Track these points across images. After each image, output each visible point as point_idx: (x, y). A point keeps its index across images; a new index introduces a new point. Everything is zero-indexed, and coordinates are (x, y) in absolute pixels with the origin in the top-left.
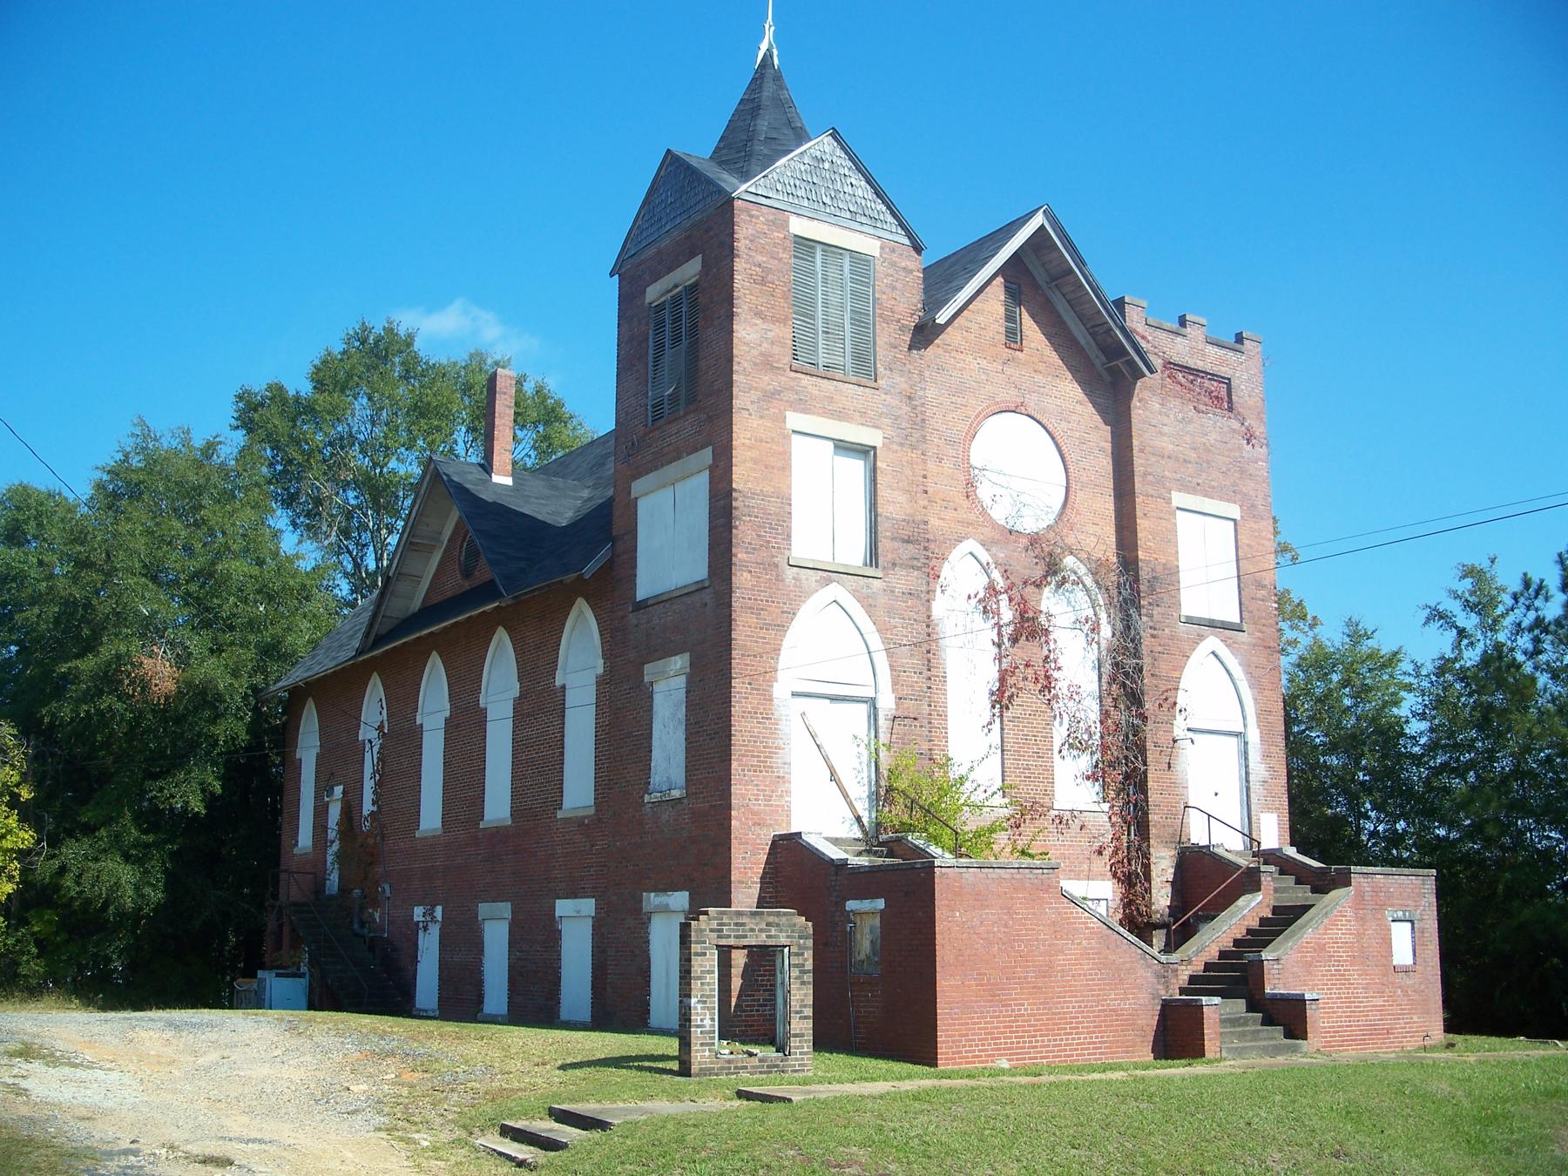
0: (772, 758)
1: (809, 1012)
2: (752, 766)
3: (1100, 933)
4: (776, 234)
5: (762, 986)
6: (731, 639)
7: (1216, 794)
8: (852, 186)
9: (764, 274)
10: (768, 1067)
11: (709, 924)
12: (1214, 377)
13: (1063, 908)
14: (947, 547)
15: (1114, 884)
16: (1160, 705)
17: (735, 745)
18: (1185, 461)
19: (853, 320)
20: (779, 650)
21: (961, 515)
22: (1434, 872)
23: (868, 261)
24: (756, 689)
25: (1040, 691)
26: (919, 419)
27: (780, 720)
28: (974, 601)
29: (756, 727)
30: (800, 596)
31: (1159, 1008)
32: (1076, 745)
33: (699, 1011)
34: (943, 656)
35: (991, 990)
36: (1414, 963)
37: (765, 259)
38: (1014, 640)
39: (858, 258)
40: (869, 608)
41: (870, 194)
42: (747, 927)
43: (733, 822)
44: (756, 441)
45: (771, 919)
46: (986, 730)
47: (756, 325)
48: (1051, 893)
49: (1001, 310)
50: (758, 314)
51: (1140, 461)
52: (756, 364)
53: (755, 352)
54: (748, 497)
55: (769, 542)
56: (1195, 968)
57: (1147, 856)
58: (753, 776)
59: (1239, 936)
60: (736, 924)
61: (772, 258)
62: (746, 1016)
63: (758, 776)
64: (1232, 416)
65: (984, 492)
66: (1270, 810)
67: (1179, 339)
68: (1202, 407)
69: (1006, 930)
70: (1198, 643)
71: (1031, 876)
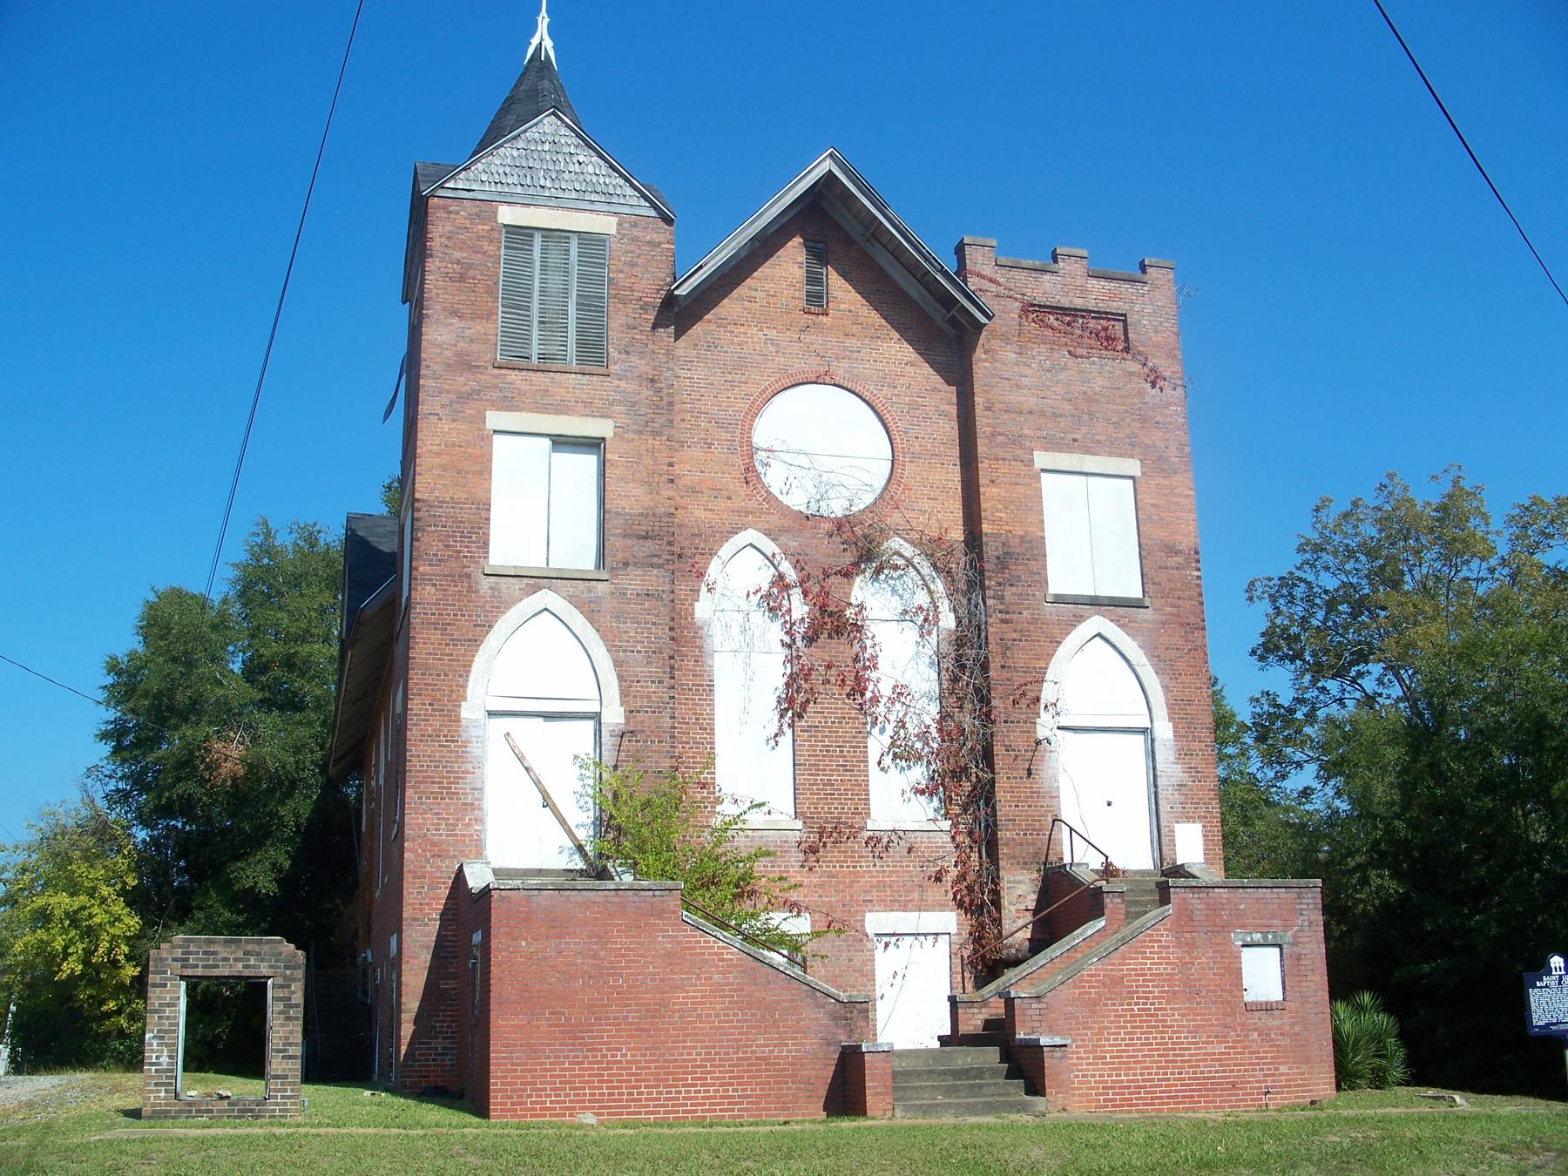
0: (458, 783)
1: (297, 1051)
2: (432, 793)
3: (742, 965)
4: (480, 227)
5: (441, 1033)
6: (408, 658)
7: (1109, 804)
8: (580, 164)
9: (463, 271)
10: (239, 1111)
11: (171, 953)
12: (1101, 315)
13: (685, 936)
15: (958, 915)
17: (410, 771)
19: (580, 306)
20: (470, 666)
21: (737, 503)
22: (1319, 882)
23: (605, 241)
24: (438, 710)
25: (848, 695)
26: (664, 403)
27: (470, 742)
28: (755, 599)
29: (438, 751)
31: (837, 1056)
32: (902, 754)
33: (155, 1047)
34: (710, 662)
35: (572, 1031)
36: (1284, 999)
37: (465, 255)
38: (810, 639)
40: (591, 615)
41: (605, 170)
42: (219, 957)
43: (406, 855)
44: (446, 446)
45: (250, 947)
46: (772, 743)
47: (451, 324)
48: (667, 918)
49: (800, 273)
50: (455, 313)
51: (985, 421)
52: (448, 365)
53: (448, 354)
54: (434, 506)
55: (459, 552)
56: (994, 1011)
57: (996, 880)
58: (433, 804)
61: (475, 252)
62: (418, 1066)
63: (439, 804)
64: (1129, 357)
65: (774, 478)
66: (1190, 819)
67: (1047, 277)
68: (1080, 351)
69: (594, 962)
70: (1075, 626)
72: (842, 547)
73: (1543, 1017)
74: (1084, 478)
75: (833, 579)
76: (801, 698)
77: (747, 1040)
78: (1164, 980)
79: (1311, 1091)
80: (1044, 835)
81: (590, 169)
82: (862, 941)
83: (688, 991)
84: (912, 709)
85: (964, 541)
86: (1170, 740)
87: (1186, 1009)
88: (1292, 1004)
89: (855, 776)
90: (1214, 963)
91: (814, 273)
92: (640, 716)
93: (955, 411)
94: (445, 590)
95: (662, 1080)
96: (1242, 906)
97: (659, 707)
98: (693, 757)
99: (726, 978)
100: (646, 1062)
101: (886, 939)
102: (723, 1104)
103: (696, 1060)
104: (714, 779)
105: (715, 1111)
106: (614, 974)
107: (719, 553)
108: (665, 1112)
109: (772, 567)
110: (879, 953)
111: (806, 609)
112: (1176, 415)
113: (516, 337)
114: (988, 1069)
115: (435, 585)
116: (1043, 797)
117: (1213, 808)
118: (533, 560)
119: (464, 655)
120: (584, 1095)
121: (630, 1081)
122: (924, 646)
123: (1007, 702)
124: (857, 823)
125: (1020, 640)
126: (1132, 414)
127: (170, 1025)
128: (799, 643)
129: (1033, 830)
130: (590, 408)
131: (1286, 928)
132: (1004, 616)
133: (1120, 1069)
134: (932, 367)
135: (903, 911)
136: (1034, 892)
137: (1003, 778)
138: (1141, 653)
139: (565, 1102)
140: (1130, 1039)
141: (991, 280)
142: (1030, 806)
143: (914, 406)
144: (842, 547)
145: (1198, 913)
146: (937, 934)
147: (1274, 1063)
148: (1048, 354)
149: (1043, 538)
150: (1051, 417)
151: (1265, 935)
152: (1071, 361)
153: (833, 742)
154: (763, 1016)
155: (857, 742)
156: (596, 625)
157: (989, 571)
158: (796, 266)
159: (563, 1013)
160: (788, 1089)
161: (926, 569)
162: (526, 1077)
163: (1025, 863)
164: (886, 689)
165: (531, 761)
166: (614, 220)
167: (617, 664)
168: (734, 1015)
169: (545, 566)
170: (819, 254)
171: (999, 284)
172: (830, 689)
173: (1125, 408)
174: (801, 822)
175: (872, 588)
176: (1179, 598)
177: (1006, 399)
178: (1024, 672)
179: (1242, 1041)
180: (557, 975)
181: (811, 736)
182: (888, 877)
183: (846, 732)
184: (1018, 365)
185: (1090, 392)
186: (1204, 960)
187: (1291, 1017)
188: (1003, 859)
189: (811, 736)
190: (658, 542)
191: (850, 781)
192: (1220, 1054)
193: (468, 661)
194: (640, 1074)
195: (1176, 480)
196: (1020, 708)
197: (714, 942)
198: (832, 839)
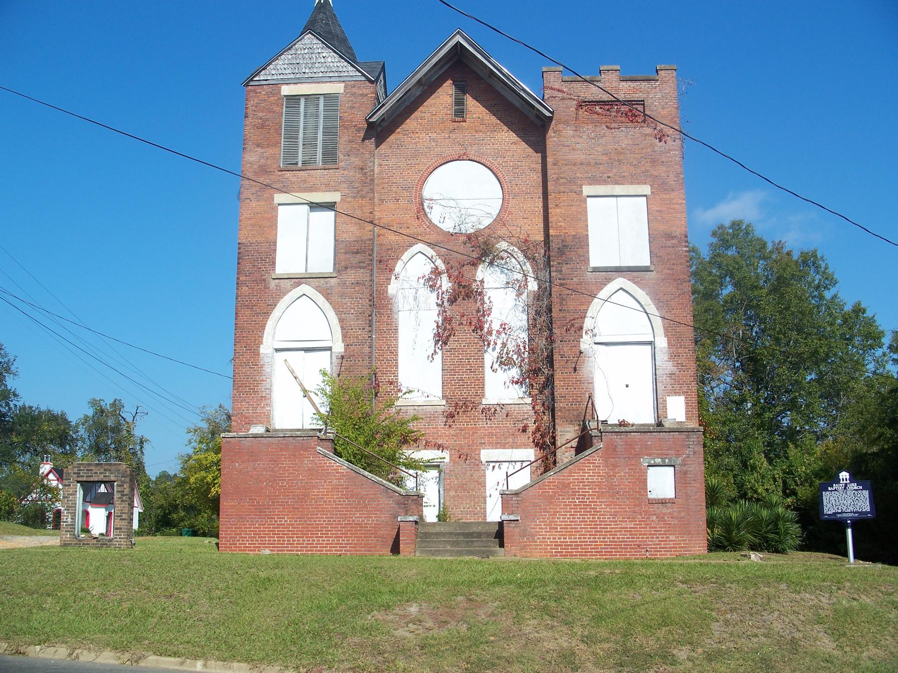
2: (245, 392)
3: (348, 475)
4: (272, 98)
7: (627, 386)
10: (101, 544)
13: (318, 460)
14: (400, 252)
15: (535, 450)
18: (596, 164)
20: (265, 326)
23: (338, 97)
24: (249, 350)
25: (473, 331)
28: (422, 281)
30: (279, 295)
32: (505, 362)
34: (396, 317)
37: (264, 114)
38: (453, 300)
39: (330, 98)
42: (93, 472)
46: (430, 359)
47: (257, 151)
51: (552, 171)
52: (256, 173)
53: (255, 167)
55: (260, 268)
60: (87, 470)
63: (249, 397)
65: (435, 215)
66: (677, 393)
68: (613, 125)
70: (605, 285)
71: (294, 441)
72: (471, 249)
73: (831, 509)
74: (615, 199)
75: (465, 267)
76: (447, 333)
77: (350, 514)
78: (596, 485)
79: (691, 551)
80: (583, 404)
81: (329, 60)
82: (478, 465)
83: (319, 489)
84: (511, 337)
85: (544, 241)
86: (665, 348)
87: (610, 502)
88: (680, 500)
89: (476, 375)
90: (629, 476)
91: (459, 99)
92: (352, 348)
93: (540, 167)
94: (253, 288)
95: (305, 534)
96: (649, 443)
97: (363, 342)
98: (386, 368)
99: (339, 482)
100: (297, 524)
101: (492, 464)
102: (337, 547)
103: (323, 524)
104: (398, 379)
105: (332, 551)
106: (281, 480)
107: (402, 258)
108: (306, 551)
109: (432, 263)
110: (489, 473)
111: (450, 284)
112: (675, 156)
113: (291, 153)
114: (484, 533)
115: (247, 286)
117: (692, 387)
118: (298, 269)
119: (262, 321)
120: (266, 541)
121: (289, 534)
122: (519, 301)
123: (562, 330)
124: (477, 400)
125: (572, 295)
126: (646, 158)
127: (72, 504)
128: (446, 304)
130: (328, 188)
131: (678, 456)
132: (562, 281)
133: (566, 535)
134: (526, 144)
135: (503, 448)
137: (559, 373)
138: (648, 298)
139: (256, 544)
140: (573, 518)
141: (558, 90)
142: (575, 389)
143: (515, 167)
144: (471, 249)
145: (619, 447)
146: (523, 461)
147: (666, 534)
148: (592, 129)
149: (587, 235)
150: (594, 166)
151: (663, 460)
152: (608, 132)
153: (464, 356)
154: (359, 501)
155: (478, 356)
156: (330, 301)
157: (553, 256)
158: (448, 96)
159: (256, 499)
160: (372, 540)
161: (521, 257)
162: (237, 531)
163: (571, 421)
164: (496, 326)
165: (297, 374)
166: (342, 85)
167: (341, 321)
168: (344, 501)
169: (304, 272)
170: (462, 88)
171: (563, 92)
172: (463, 328)
173: (641, 155)
174: (445, 401)
175: (490, 270)
176: (674, 264)
177: (567, 157)
178: (573, 313)
179: (645, 521)
180: (253, 480)
181: (451, 354)
182: (495, 430)
183: (472, 351)
184: (574, 137)
185: (619, 148)
186: (622, 474)
187: (679, 508)
188: (558, 419)
189: (451, 354)
190: (364, 255)
191: (474, 377)
192: (630, 528)
193: (264, 324)
194: (294, 531)
195: (674, 195)
196: (570, 333)
197: (334, 463)
198: (462, 410)
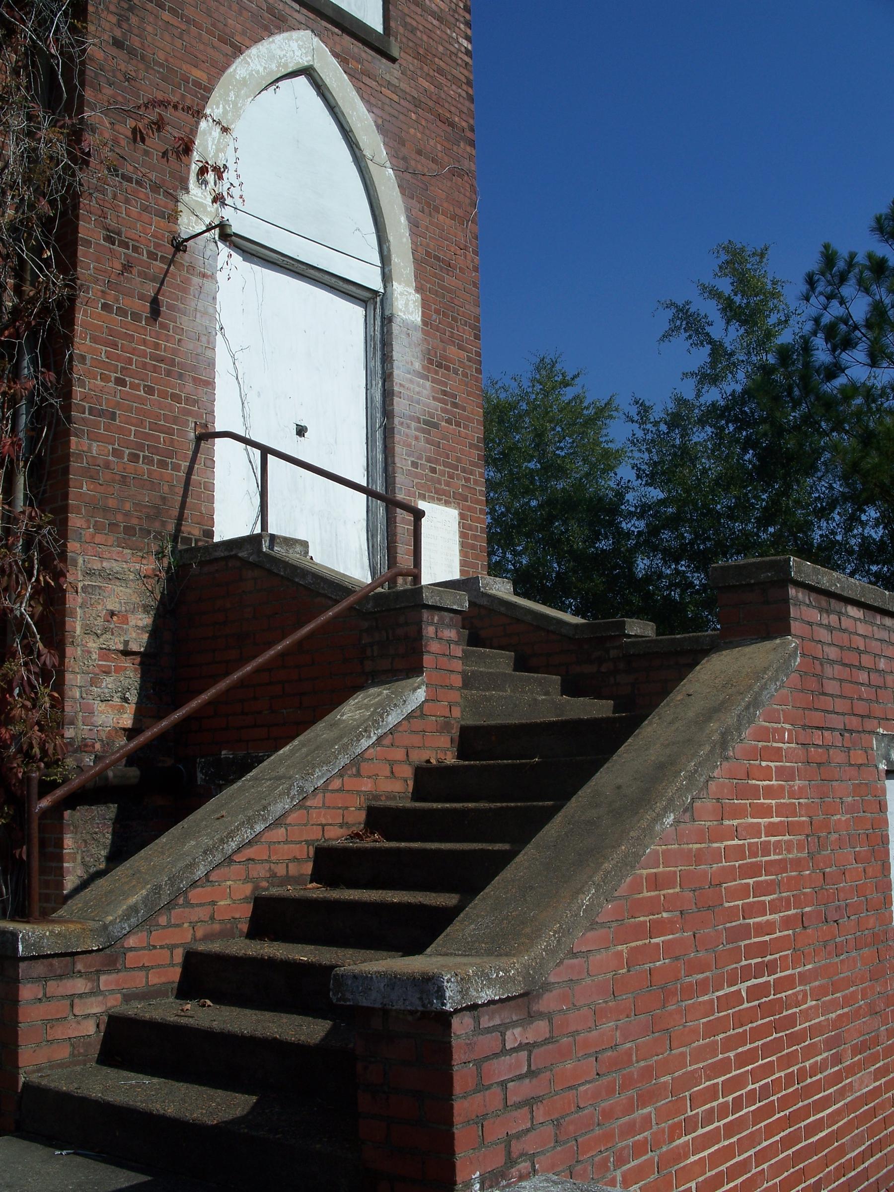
16: (137, 136)
56: (138, 981)
59: (336, 836)
66: (443, 497)
116: (181, 376)
129: (155, 450)
136: (146, 608)
142: (150, 390)
163: (129, 530)
